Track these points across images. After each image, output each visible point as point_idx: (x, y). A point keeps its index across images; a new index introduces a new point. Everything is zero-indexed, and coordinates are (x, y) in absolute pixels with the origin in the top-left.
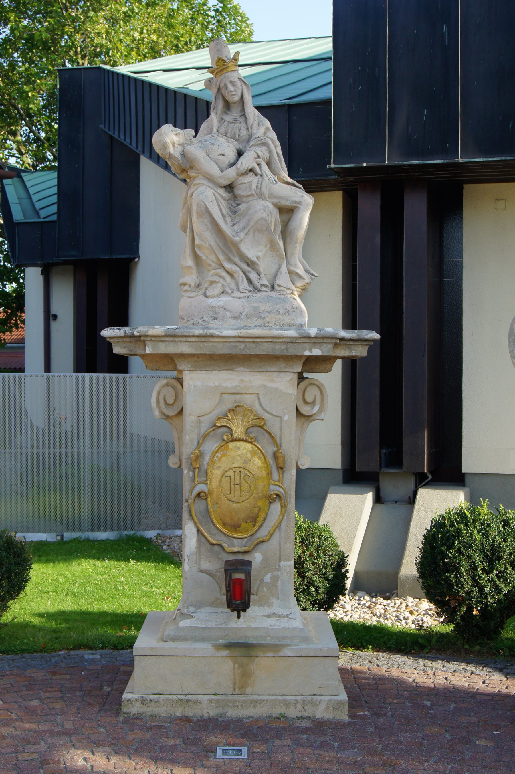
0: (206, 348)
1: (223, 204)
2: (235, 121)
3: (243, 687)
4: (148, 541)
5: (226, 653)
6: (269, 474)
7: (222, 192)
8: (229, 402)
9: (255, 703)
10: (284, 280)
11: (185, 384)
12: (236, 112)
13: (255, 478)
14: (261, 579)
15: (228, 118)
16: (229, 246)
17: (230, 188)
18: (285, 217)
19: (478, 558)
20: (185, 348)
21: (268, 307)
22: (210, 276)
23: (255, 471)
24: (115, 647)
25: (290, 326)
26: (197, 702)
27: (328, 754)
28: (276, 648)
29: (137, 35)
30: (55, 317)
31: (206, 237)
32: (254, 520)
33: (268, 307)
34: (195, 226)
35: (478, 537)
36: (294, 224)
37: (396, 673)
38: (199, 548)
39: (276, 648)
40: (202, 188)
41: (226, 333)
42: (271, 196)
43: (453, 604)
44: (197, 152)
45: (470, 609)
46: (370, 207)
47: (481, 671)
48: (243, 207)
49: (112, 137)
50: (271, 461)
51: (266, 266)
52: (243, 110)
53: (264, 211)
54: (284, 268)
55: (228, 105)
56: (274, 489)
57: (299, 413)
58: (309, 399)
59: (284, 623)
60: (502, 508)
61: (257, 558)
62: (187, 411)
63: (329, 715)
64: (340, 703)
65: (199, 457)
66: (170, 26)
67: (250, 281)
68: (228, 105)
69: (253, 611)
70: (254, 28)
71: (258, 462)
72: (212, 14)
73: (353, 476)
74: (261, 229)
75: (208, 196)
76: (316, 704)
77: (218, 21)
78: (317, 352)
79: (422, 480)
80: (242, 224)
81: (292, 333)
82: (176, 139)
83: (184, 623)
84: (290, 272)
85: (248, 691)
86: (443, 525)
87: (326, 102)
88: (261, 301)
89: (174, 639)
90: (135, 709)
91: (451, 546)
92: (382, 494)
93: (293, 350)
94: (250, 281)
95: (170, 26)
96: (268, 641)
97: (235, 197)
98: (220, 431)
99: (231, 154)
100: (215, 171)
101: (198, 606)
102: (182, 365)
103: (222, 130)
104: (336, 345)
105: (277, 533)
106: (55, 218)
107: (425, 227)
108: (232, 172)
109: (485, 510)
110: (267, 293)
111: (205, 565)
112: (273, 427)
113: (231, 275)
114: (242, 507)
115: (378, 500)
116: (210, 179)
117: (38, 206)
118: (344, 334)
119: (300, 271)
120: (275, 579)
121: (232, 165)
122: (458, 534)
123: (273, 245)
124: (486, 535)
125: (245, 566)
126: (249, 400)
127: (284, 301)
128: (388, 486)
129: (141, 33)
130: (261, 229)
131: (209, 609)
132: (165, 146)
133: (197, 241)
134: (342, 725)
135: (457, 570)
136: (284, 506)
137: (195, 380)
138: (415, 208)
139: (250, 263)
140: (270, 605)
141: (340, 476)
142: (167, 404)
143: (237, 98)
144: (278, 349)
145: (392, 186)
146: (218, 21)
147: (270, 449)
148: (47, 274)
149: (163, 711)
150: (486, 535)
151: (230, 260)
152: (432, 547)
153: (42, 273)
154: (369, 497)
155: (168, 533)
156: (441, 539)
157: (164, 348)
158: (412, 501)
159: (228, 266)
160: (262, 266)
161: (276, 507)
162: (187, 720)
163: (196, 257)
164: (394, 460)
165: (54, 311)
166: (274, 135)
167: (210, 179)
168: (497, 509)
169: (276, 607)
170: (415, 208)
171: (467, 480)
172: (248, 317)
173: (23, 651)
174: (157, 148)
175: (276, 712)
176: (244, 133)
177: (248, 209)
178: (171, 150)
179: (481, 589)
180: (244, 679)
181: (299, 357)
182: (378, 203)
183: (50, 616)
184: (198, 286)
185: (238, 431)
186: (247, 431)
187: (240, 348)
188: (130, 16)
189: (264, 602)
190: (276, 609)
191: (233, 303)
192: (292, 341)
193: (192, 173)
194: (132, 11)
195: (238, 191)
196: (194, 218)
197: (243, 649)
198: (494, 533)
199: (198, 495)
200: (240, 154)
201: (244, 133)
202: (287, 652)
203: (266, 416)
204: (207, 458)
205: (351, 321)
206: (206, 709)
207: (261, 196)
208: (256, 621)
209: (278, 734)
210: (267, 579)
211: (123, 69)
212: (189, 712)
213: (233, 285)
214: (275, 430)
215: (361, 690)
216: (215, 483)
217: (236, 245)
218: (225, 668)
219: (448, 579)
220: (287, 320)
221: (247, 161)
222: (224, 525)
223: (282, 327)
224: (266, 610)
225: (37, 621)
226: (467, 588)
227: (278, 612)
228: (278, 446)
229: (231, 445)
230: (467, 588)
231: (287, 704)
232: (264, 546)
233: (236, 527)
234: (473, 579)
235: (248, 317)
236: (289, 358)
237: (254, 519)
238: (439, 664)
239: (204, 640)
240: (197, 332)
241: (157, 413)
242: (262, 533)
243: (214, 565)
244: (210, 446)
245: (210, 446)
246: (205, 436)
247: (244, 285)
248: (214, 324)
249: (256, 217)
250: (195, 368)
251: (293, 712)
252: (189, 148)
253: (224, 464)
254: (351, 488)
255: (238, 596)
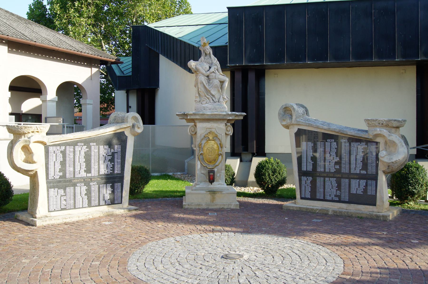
0: (203, 117)
1: (206, 80)
2: (208, 59)
3: (213, 201)
4: (170, 176)
5: (209, 193)
6: (219, 149)
7: (206, 77)
8: (208, 131)
9: (216, 205)
10: (221, 100)
11: (197, 126)
12: (208, 56)
13: (215, 150)
14: (217, 175)
15: (206, 58)
16: (208, 91)
17: (208, 76)
18: (222, 83)
19: (270, 172)
20: (198, 117)
21: (218, 107)
22: (203, 99)
23: (215, 148)
24: (174, 197)
25: (223, 112)
26: (202, 205)
27: (235, 214)
28: (221, 192)
29: (153, 11)
30: (130, 107)
31: (202, 89)
32: (215, 160)
33: (218, 107)
34: (199, 86)
35: (270, 166)
36: (223, 86)
37: (249, 201)
38: (201, 168)
39: (221, 192)
40: (201, 77)
41: (208, 113)
42: (218, 78)
43: (264, 184)
44: (200, 67)
45: (268, 185)
46: (239, 76)
47: (271, 200)
48: (211, 81)
49: (150, 48)
50: (219, 145)
51: (217, 96)
52: (210, 56)
53: (217, 82)
54: (221, 97)
55: (206, 54)
56: (220, 153)
57: (226, 134)
58: (228, 130)
59: (222, 186)
60: (276, 159)
61: (216, 170)
62: (198, 133)
63: (235, 208)
64: (237, 205)
65: (201, 144)
66: (164, 7)
67: (213, 100)
68: (206, 54)
69: (214, 183)
70: (192, 7)
71: (216, 146)
72: (178, 3)
73: (234, 154)
74: (216, 87)
75: (203, 79)
76: (231, 205)
77: (180, 5)
78: (231, 118)
79: (254, 155)
80: (211, 86)
81: (224, 113)
82: (194, 64)
83: (197, 186)
84: (223, 98)
85: (214, 202)
86: (261, 164)
87: (227, 46)
88: (216, 105)
89: (195, 190)
90: (186, 207)
91: (263, 169)
92: (242, 159)
93: (225, 118)
94: (213, 100)
95: (164, 7)
96: (219, 190)
97: (209, 79)
98: (206, 138)
99: (208, 68)
100: (204, 72)
101: (201, 182)
102: (196, 121)
103: (205, 61)
104: (235, 116)
105: (220, 164)
106: (131, 74)
107: (254, 82)
108: (208, 73)
109: (272, 160)
110: (218, 103)
111: (203, 172)
112: (220, 137)
113: (208, 98)
114: (212, 157)
115: (241, 161)
116: (203, 74)
117: (123, 70)
118: (230, 113)
119: (225, 97)
120: (220, 175)
121: (208, 71)
122: (265, 166)
123: (219, 91)
124: (273, 166)
125: (213, 172)
126: (213, 130)
127: (222, 105)
128: (244, 157)
129: (155, 10)
130: (216, 87)
131: (204, 183)
132: (191, 66)
133: (199, 90)
134: (238, 209)
135: (265, 175)
136: (222, 157)
137: (200, 125)
138: (252, 76)
139: (213, 96)
140: (219, 182)
141: (230, 154)
142: (192, 131)
143: (208, 53)
144: (221, 117)
145: (245, 71)
146: (180, 5)
147: (219, 142)
148: (127, 93)
149: (193, 207)
150: (273, 166)
151: (208, 95)
152: (259, 170)
153: (126, 92)
154: (239, 160)
155: (175, 173)
156: (260, 168)
157: (192, 117)
158: (251, 161)
159: (207, 96)
160: (216, 96)
161: (220, 157)
162: (199, 209)
163: (199, 94)
164: (246, 149)
165: (130, 105)
166: (218, 62)
167: (203, 74)
168: (275, 160)
169: (220, 182)
170: (252, 76)
171: (267, 155)
172: (213, 109)
173: (150, 198)
174: (189, 66)
175: (221, 207)
176: (211, 62)
177: (212, 82)
178: (193, 67)
179: (271, 180)
180: (213, 199)
181: (226, 119)
182: (241, 75)
183: (153, 191)
184: (200, 101)
185: (211, 138)
186: (213, 138)
187: (212, 117)
188: (151, 5)
189: (218, 181)
190: (220, 183)
191: (209, 106)
192: (225, 115)
193: (198, 73)
194: (152, 3)
195: (210, 77)
196: (199, 84)
197: (213, 192)
198: (274, 166)
199: (201, 154)
200: (210, 68)
201: (211, 62)
202: (224, 192)
203: (218, 134)
204: (203, 145)
205: (233, 109)
206: (204, 207)
207: (216, 78)
208: (216, 185)
209: (223, 211)
210: (218, 175)
211: (152, 25)
212: (200, 207)
213: (209, 101)
214: (220, 138)
215: (242, 204)
216: (205, 151)
217: (210, 91)
218: (208, 197)
219: (262, 178)
220: (223, 110)
221: (212, 70)
222: (207, 162)
223: (222, 112)
224: (218, 183)
225: (150, 192)
226: (268, 180)
227: (220, 184)
228: (221, 142)
229: (209, 141)
230: (268, 180)
231: (224, 205)
232: (217, 167)
233: (210, 162)
234: (269, 178)
235: (213, 109)
236: (223, 120)
237: (215, 160)
238: (260, 199)
239: (203, 190)
240: (201, 113)
241: (189, 134)
242: (217, 164)
243: (205, 172)
244: (204, 142)
245: (204, 142)
246: (202, 139)
247: (212, 101)
248: (204, 111)
249: (215, 84)
250: (200, 122)
251: (226, 207)
252: (197, 66)
253: (207, 146)
254: (233, 158)
255: (212, 180)
